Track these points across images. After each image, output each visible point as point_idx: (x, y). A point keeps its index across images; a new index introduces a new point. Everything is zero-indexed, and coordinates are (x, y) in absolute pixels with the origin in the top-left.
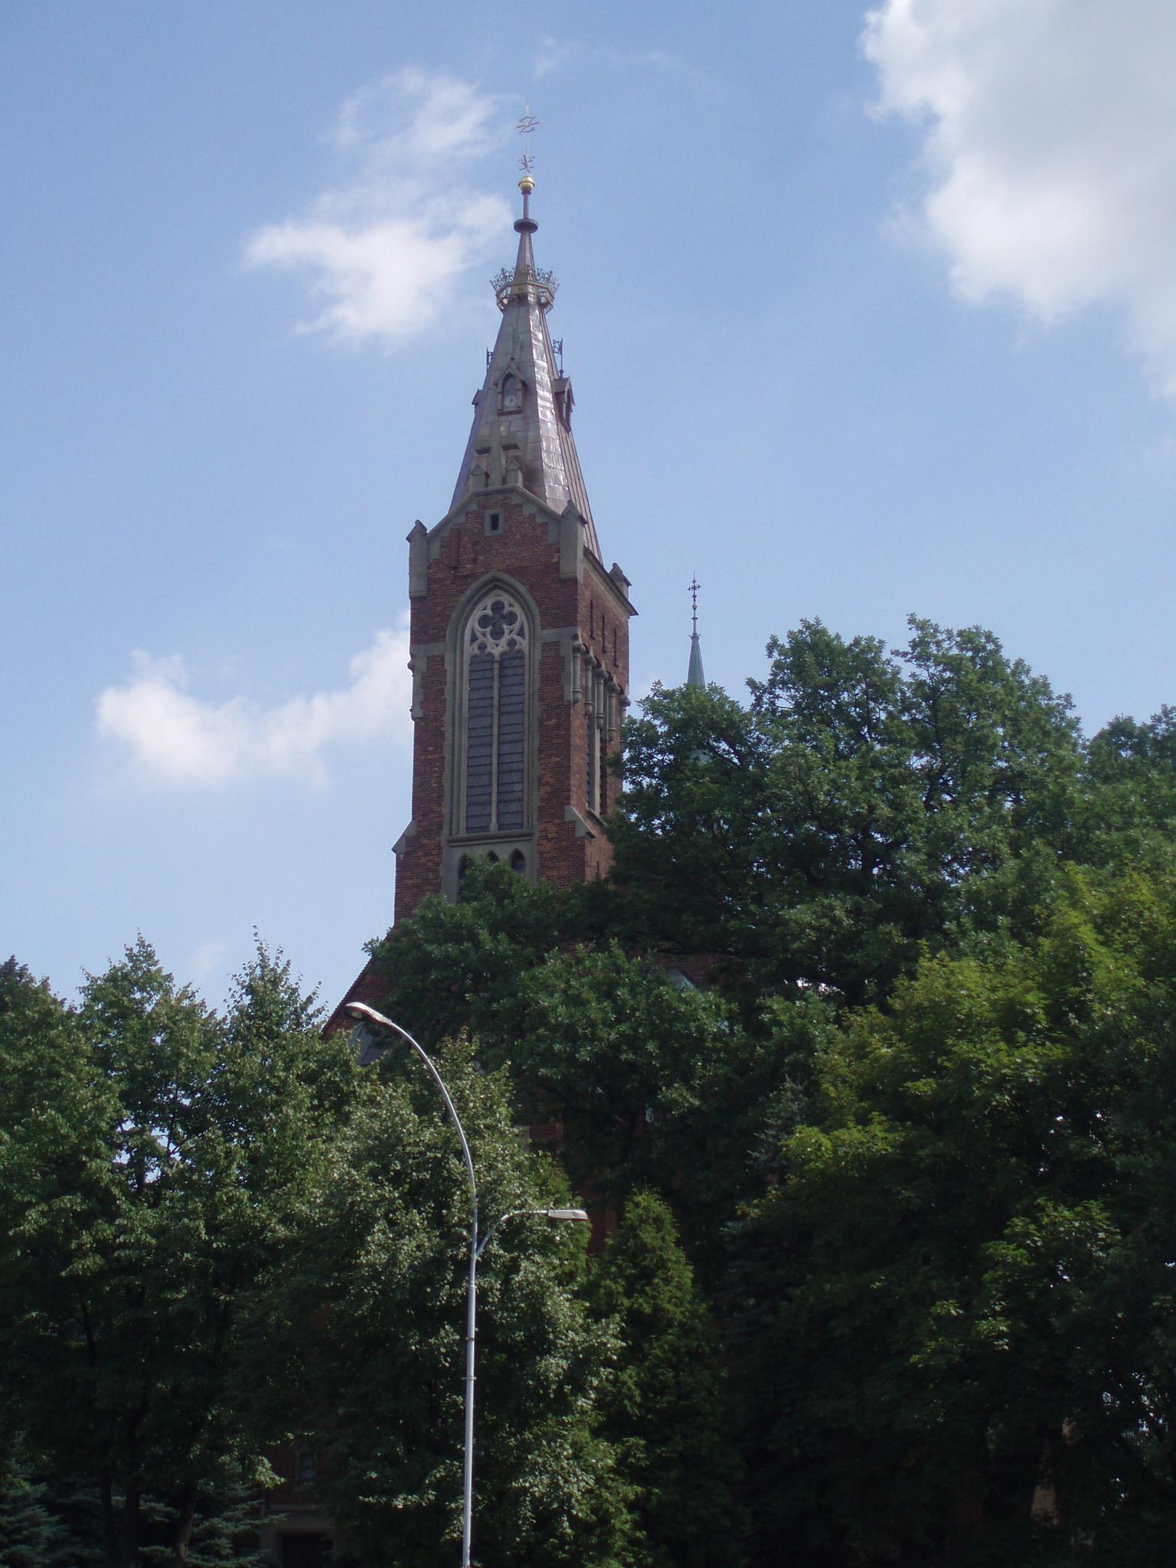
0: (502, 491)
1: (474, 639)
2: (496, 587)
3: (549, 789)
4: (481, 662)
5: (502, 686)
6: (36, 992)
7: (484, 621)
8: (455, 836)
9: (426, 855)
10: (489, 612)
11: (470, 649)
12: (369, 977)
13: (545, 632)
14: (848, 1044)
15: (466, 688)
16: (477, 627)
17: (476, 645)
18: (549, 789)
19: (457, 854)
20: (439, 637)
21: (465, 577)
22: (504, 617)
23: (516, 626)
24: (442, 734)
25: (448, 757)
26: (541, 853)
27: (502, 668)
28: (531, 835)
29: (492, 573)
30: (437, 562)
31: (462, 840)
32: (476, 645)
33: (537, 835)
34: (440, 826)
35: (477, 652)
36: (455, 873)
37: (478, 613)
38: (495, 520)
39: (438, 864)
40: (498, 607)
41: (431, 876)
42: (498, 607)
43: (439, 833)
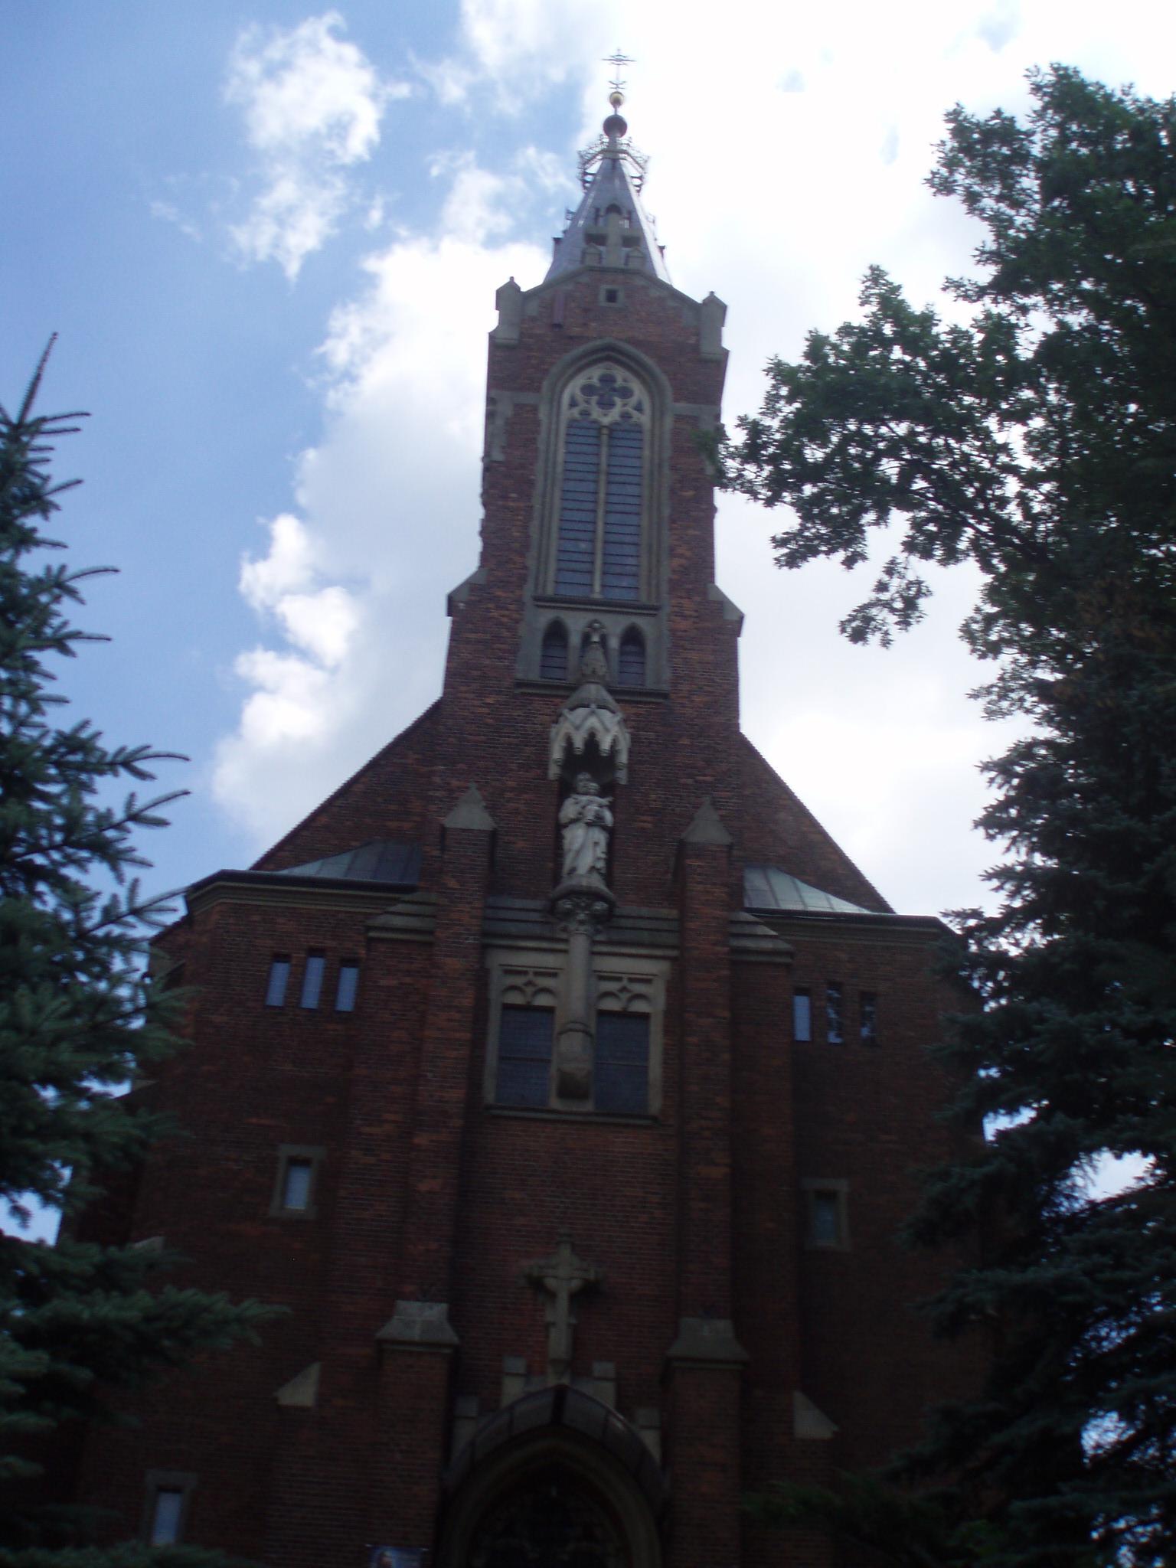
0: (623, 271)
1: (573, 404)
2: (608, 358)
3: (683, 561)
4: (583, 430)
5: (610, 456)
6: (323, 364)
7: (588, 390)
8: (540, 591)
10: (595, 381)
11: (567, 413)
12: (323, 820)
13: (678, 405)
14: (1066, 1204)
15: (562, 451)
16: (578, 393)
17: (576, 412)
18: (683, 561)
19: (544, 618)
20: (534, 386)
21: (571, 338)
22: (614, 390)
23: (633, 401)
24: (531, 484)
25: (537, 507)
26: (673, 631)
27: (611, 437)
28: (657, 609)
29: (608, 340)
30: (533, 319)
31: (552, 600)
32: (576, 412)
33: (667, 610)
34: (523, 579)
35: (577, 416)
36: (539, 638)
37: (580, 381)
38: (612, 297)
39: (517, 621)
40: (607, 380)
41: (505, 633)
42: (607, 380)
43: (520, 587)
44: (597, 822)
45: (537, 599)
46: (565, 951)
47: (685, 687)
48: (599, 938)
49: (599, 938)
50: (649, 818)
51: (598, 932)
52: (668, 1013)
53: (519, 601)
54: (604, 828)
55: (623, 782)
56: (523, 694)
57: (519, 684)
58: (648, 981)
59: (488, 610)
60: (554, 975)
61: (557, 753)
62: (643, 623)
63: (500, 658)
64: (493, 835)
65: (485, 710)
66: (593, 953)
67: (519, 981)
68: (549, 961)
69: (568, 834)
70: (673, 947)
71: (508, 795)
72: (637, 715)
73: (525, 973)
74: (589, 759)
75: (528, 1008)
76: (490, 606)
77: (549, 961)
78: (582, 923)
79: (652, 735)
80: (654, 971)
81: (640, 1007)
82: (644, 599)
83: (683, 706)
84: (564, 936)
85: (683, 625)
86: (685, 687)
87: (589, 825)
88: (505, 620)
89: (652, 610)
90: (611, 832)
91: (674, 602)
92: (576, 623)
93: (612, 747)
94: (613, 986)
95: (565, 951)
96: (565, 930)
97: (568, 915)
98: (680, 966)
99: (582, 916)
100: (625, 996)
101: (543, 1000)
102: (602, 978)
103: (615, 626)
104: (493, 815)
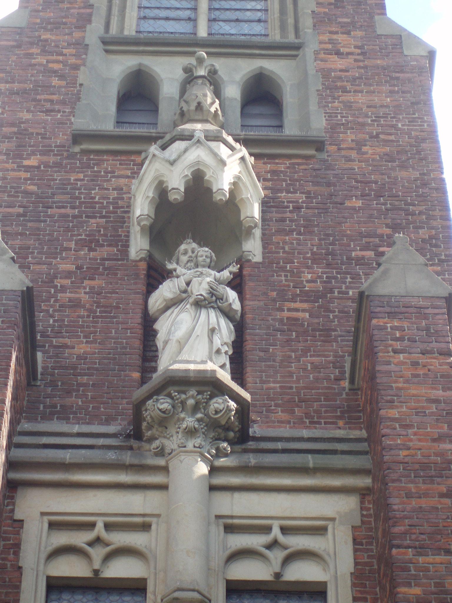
8: (114, 30)
9: (44, 52)
19: (120, 66)
26: (326, 74)
28: (298, 47)
33: (309, 52)
36: (113, 92)
39: (76, 67)
43: (81, 27)
44: (211, 301)
45: (105, 42)
46: (163, 487)
47: (349, 137)
48: (222, 461)
49: (222, 461)
50: (305, 306)
51: (220, 453)
52: (359, 577)
53: (82, 47)
54: (227, 314)
55: (258, 258)
56: (84, 152)
57: (78, 138)
58: (320, 531)
59: (30, 56)
60: (146, 527)
61: (142, 207)
62: (278, 68)
63: (48, 112)
64: (28, 298)
65: (23, 175)
66: (213, 488)
67: (80, 539)
68: (135, 503)
69: (162, 326)
70: (365, 472)
71: (58, 282)
72: (274, 172)
73: (92, 526)
74: (194, 215)
75: (95, 586)
76: (35, 50)
77: (135, 503)
78: (191, 433)
79: (301, 198)
80: (329, 512)
81: (303, 572)
82: (276, 37)
83: (349, 159)
84: (161, 462)
85: (340, 63)
86: (349, 137)
87: (199, 304)
88: (56, 66)
89: (290, 50)
90: (240, 328)
91: (325, 37)
92: (167, 73)
93: (231, 192)
94: (256, 541)
95: (163, 487)
96: (161, 452)
97: (164, 421)
98: (375, 502)
99: (190, 421)
100: (276, 556)
101: (121, 569)
102: (230, 529)
103: (235, 73)
104: (23, 267)
